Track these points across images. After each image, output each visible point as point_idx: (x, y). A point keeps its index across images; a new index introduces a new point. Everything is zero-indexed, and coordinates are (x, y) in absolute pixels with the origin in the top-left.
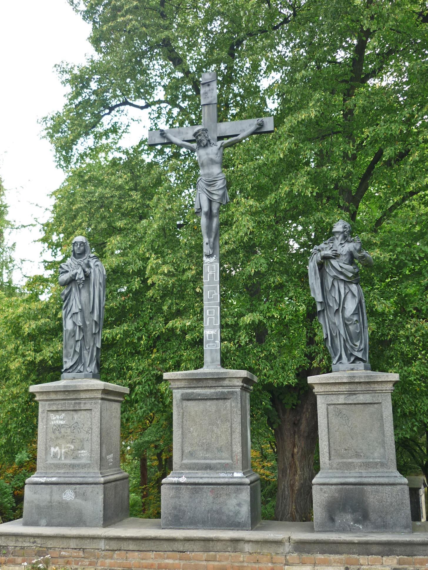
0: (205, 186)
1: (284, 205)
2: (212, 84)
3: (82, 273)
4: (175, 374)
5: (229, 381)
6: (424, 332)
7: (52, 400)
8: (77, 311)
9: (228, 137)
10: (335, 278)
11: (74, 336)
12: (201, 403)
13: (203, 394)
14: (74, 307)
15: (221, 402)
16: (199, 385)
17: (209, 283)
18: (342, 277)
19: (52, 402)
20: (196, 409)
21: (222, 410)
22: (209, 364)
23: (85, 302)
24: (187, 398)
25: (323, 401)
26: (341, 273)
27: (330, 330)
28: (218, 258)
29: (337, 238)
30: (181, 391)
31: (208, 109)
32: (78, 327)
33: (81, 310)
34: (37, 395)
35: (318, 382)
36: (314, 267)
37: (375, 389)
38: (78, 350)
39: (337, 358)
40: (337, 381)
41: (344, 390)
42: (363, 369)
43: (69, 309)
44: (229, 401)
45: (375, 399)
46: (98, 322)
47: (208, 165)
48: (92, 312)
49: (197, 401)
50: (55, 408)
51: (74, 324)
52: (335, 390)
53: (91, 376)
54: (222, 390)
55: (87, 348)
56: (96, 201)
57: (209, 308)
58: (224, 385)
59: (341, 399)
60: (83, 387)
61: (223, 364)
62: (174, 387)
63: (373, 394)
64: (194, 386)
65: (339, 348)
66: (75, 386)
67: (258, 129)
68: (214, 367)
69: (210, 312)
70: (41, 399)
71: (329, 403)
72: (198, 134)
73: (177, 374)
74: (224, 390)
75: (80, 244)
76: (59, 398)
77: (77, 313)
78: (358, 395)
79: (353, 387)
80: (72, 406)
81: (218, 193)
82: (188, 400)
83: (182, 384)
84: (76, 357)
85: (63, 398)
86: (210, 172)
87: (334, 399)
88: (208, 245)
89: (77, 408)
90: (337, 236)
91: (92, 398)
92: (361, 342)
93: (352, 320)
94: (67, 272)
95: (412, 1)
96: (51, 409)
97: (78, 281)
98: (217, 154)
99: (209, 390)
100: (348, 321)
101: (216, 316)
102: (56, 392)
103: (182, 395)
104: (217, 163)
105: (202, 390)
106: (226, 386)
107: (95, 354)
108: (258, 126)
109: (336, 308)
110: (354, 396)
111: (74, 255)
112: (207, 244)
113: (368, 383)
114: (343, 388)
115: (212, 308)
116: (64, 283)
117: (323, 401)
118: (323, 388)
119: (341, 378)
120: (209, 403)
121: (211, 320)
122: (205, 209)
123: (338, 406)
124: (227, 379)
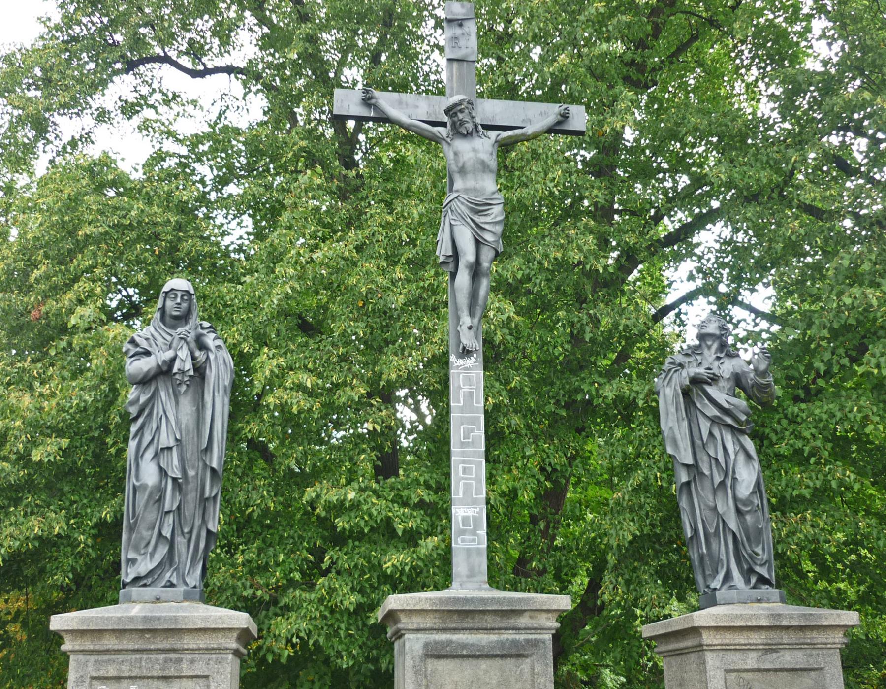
0: (467, 211)
1: (540, 284)
2: (466, 23)
4: (415, 598)
5: (531, 617)
6: (802, 536)
7: (107, 652)
8: (172, 443)
10: (714, 420)
11: (161, 500)
12: (466, 663)
13: (473, 645)
15: (510, 663)
16: (466, 625)
17: (462, 410)
18: (729, 421)
19: (106, 657)
20: (456, 678)
21: (513, 680)
22: (465, 579)
23: (187, 426)
24: (435, 653)
25: (717, 664)
26: (727, 412)
27: (703, 520)
28: (481, 359)
29: (709, 347)
30: (423, 637)
31: (459, 70)
32: (170, 482)
34: (67, 638)
35: (713, 624)
36: (676, 396)
37: (815, 641)
38: (167, 533)
39: (721, 576)
40: (749, 624)
41: (759, 641)
42: (778, 600)
44: (528, 660)
45: (811, 661)
47: (474, 171)
48: (209, 448)
49: (457, 661)
50: (112, 671)
51: (163, 472)
52: (743, 642)
53: (198, 597)
54: (514, 636)
55: (186, 530)
56: (130, 227)
57: (464, 462)
58: (520, 626)
59: (751, 661)
60: (194, 623)
61: (493, 580)
62: (410, 627)
63: (808, 652)
64: (454, 626)
65: (723, 557)
66: (175, 619)
67: (559, 123)
68: (476, 585)
69: (464, 469)
70: (77, 648)
71: (729, 667)
72: (459, 108)
73: (420, 600)
74: (517, 637)
75: (182, 296)
76: (125, 647)
77: (169, 449)
78: (782, 653)
79: (774, 636)
80: (157, 667)
81: (493, 230)
82: (439, 657)
83: (429, 621)
84: (163, 550)
85: (136, 647)
86: (478, 186)
87: (737, 660)
88: (472, 332)
89: (172, 672)
90: (709, 343)
91: (213, 649)
92: (763, 549)
93: (752, 503)
94: (147, 353)
96: (102, 673)
97: (177, 377)
98: (492, 154)
99: (486, 636)
100: (745, 505)
101: (478, 481)
102: (120, 633)
103: (426, 645)
104: (491, 171)
105: (469, 636)
106: (525, 629)
107: (202, 545)
108: (559, 118)
109: (718, 479)
110: (775, 655)
111: (163, 319)
112: (470, 328)
113: (801, 628)
114: (756, 638)
115: (470, 462)
116: (140, 377)
117: (717, 664)
118: (718, 637)
119: (757, 617)
120: (484, 664)
121: (467, 487)
122: (468, 254)
123: (744, 675)
124: (527, 614)
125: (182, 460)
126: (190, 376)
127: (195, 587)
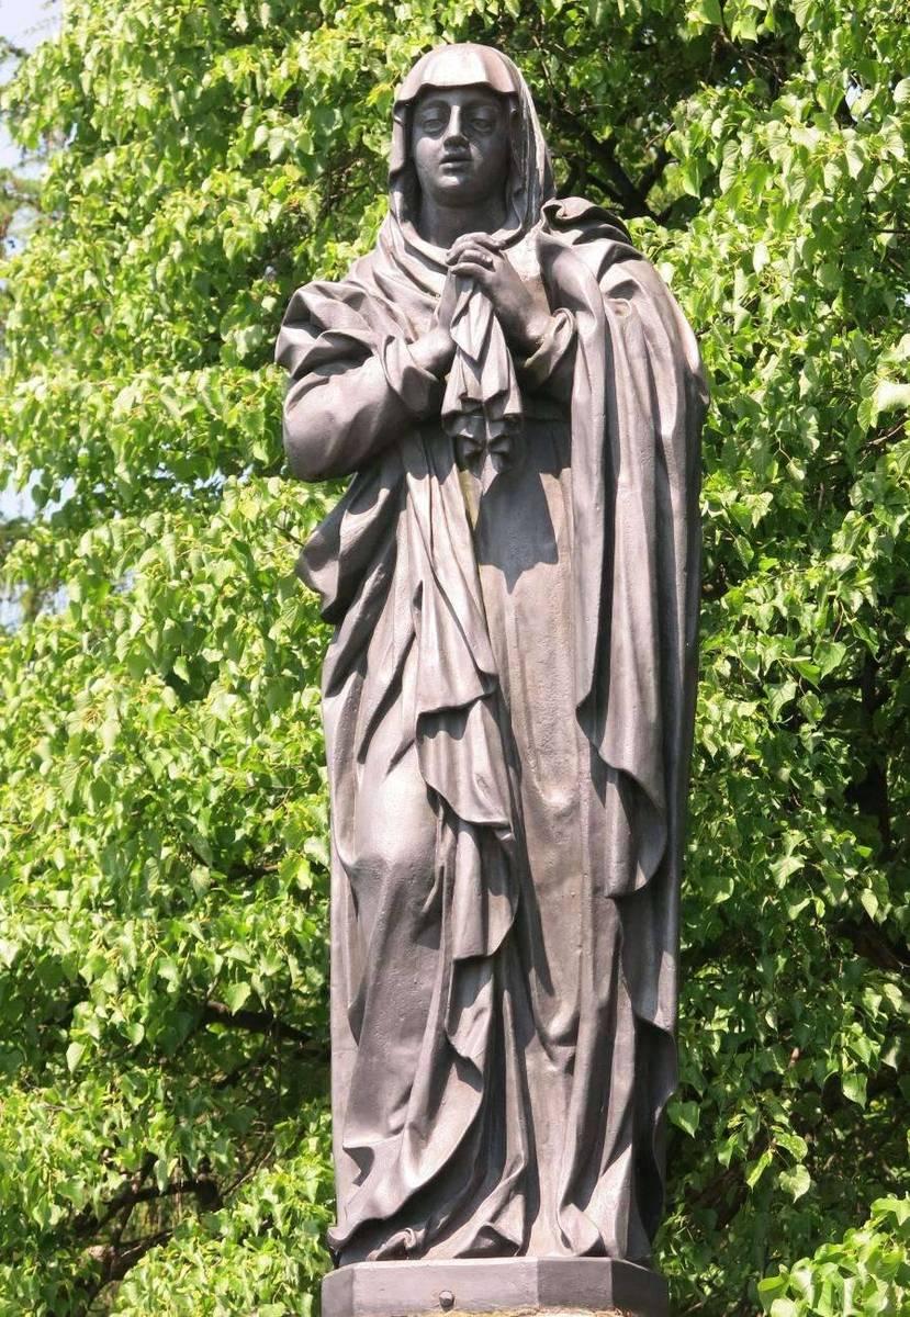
3: (499, 349)
9: (373, 1001)
11: (430, 925)
14: (425, 658)
32: (467, 841)
33: (493, 691)
38: (471, 1042)
43: (381, 676)
46: (655, 793)
48: (593, 710)
84: (462, 1105)
94: (354, 353)
95: (900, 584)
107: (622, 1082)
125: (510, 754)
126: (509, 421)
127: (598, 1250)
